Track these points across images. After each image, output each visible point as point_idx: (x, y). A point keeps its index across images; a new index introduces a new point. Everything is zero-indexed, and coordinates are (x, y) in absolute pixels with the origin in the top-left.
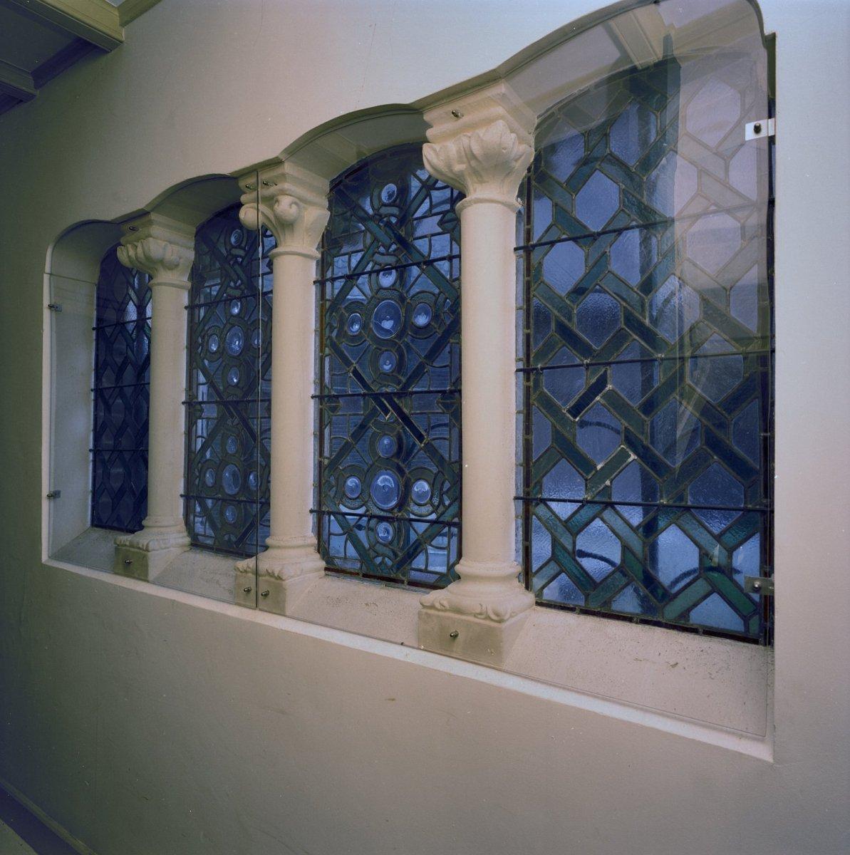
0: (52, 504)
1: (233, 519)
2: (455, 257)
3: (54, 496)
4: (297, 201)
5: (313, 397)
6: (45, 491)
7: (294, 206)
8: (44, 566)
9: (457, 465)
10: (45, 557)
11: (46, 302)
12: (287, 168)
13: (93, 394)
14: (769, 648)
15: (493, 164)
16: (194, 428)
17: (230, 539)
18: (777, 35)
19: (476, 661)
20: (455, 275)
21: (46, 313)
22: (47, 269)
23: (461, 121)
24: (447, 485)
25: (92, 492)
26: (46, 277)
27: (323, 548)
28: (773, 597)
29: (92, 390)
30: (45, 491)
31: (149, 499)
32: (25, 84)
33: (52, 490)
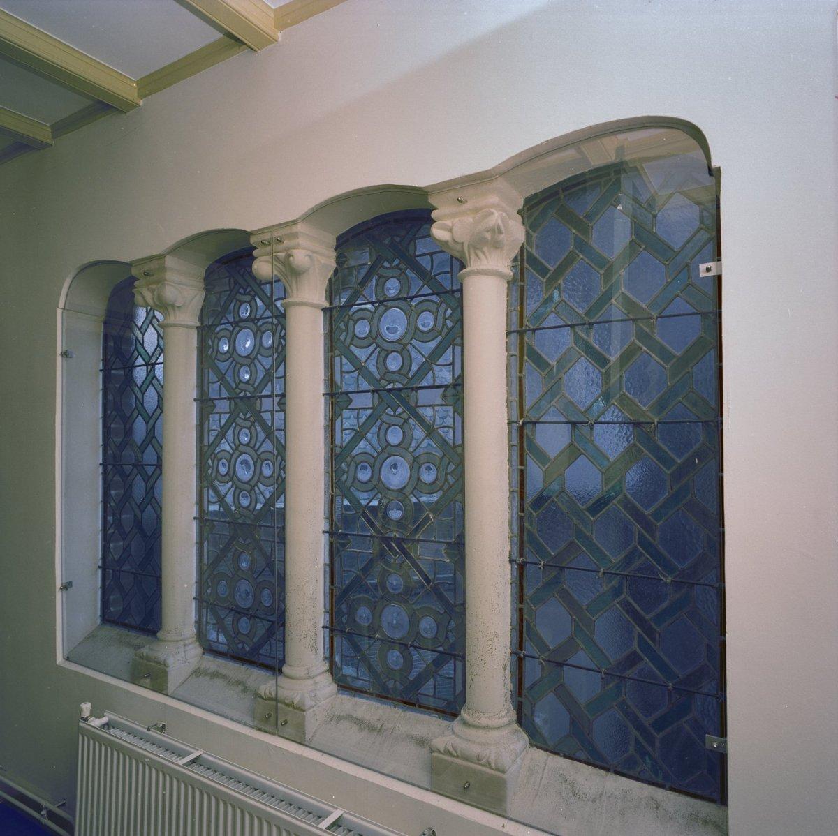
0: (64, 595)
1: (250, 633)
2: (458, 385)
3: (66, 587)
4: (311, 254)
5: (323, 395)
6: (58, 584)
7: (307, 258)
8: (59, 668)
9: (460, 448)
10: (59, 659)
11: (59, 351)
12: (299, 228)
13: (101, 373)
14: (723, 808)
15: (489, 240)
16: (207, 422)
17: (243, 648)
18: (721, 169)
19: (478, 805)
20: (459, 442)
21: (59, 359)
22: (61, 305)
23: (465, 206)
24: (452, 467)
25: (102, 559)
26: (59, 312)
27: (333, 670)
28: (726, 754)
29: (101, 370)
30: (58, 584)
31: (163, 599)
32: (44, 134)
33: (64, 581)
